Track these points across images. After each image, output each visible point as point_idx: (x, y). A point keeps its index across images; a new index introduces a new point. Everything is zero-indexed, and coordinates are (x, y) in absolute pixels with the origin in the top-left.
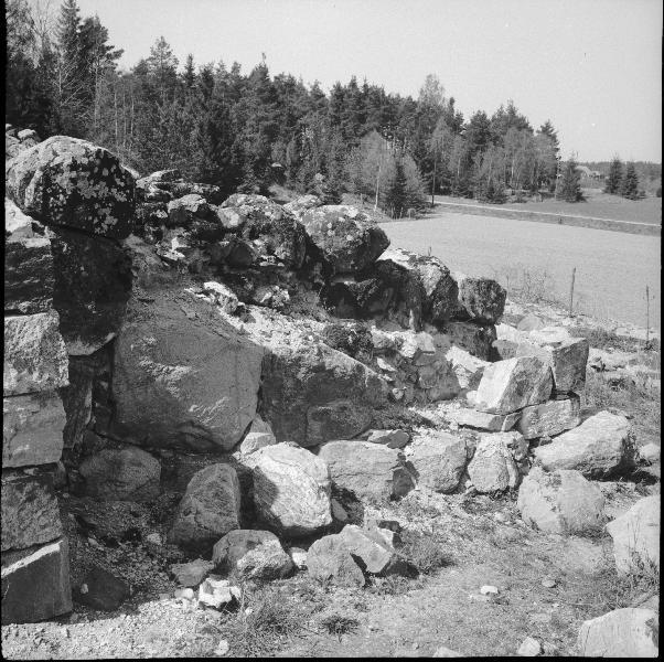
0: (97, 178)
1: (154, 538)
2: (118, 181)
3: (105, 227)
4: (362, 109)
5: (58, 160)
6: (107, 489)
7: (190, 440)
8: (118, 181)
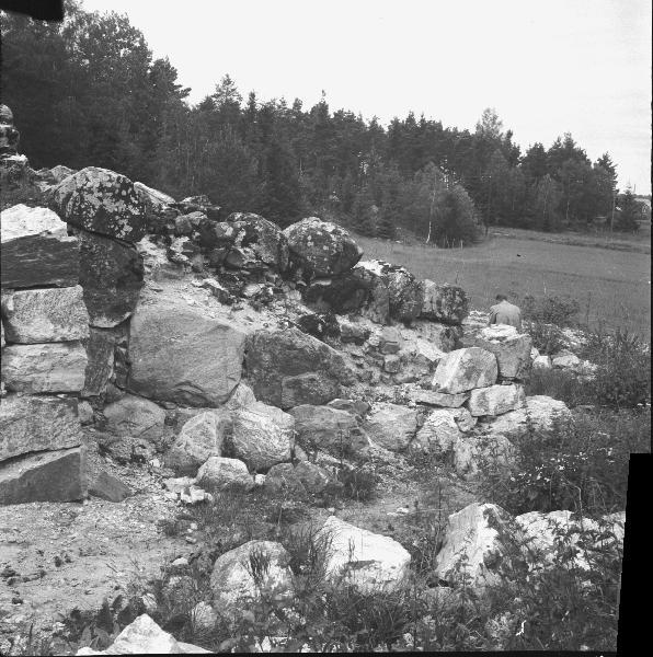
0: (117, 197)
1: (156, 462)
2: (133, 199)
3: (124, 234)
5: (89, 184)
6: (123, 428)
7: (188, 396)
8: (133, 199)
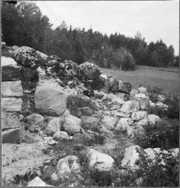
0: (32, 55)
1: (41, 132)
2: (36, 56)
4: (117, 41)
5: (23, 51)
7: (51, 113)
8: (36, 56)
